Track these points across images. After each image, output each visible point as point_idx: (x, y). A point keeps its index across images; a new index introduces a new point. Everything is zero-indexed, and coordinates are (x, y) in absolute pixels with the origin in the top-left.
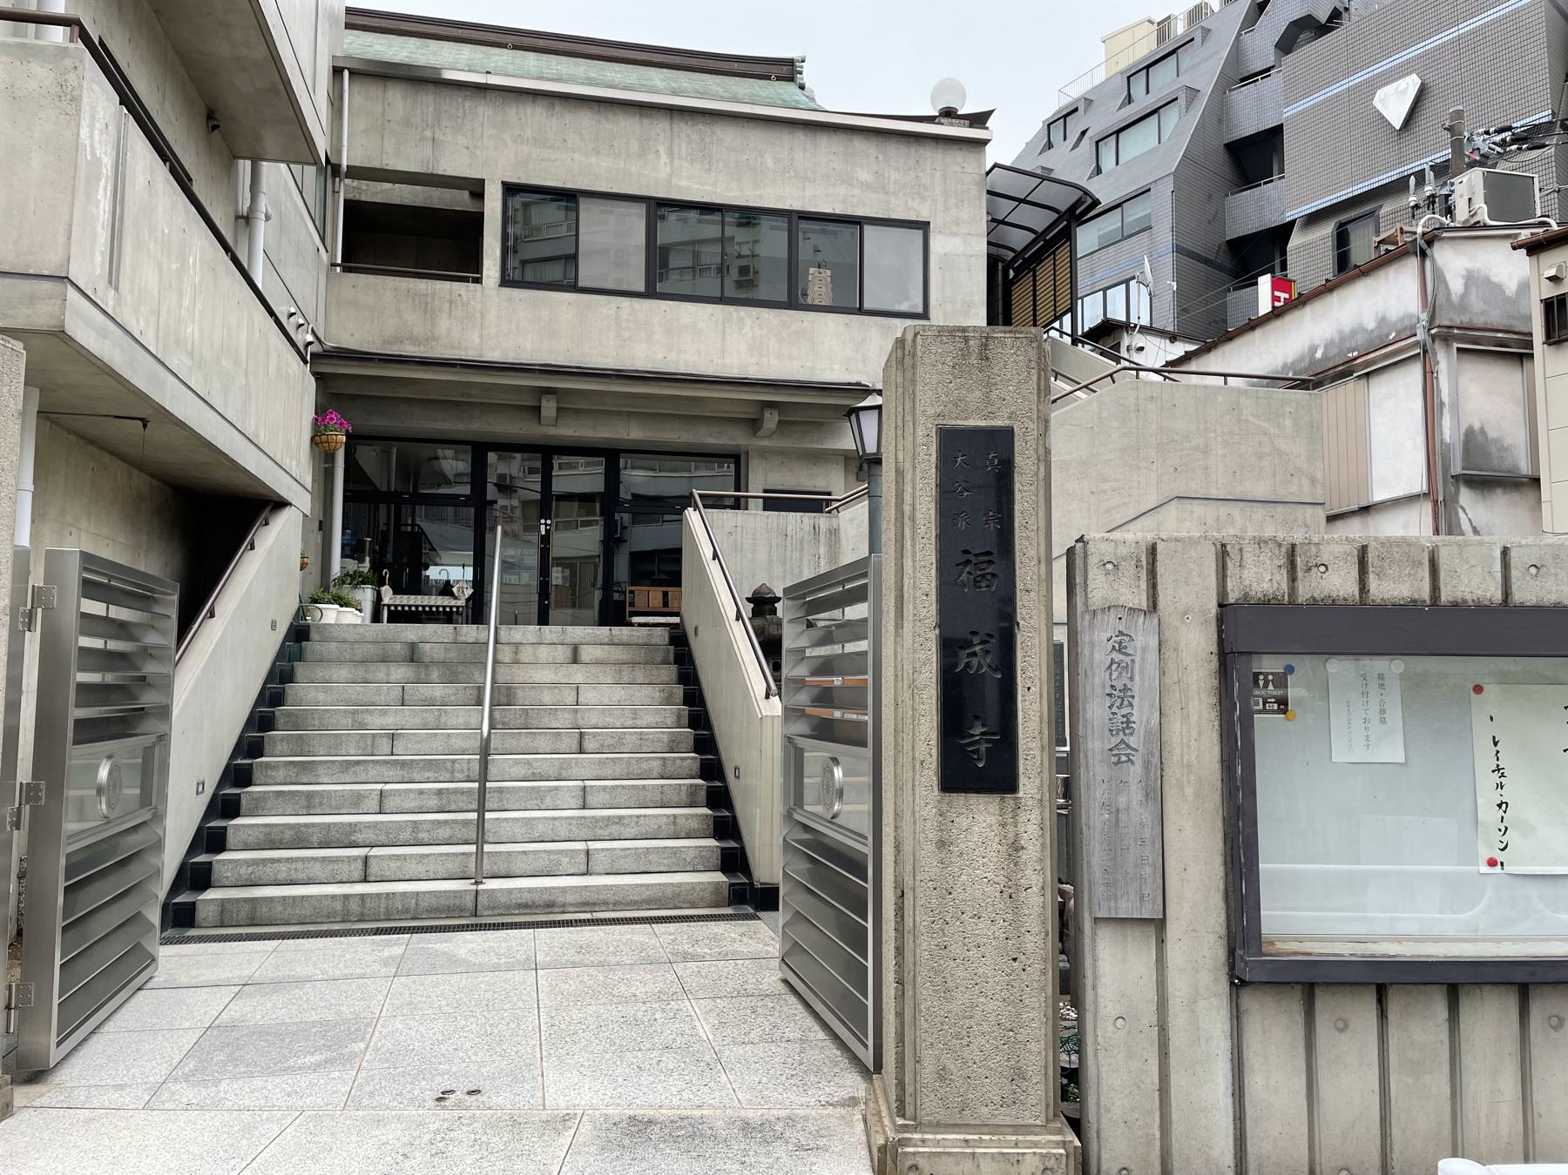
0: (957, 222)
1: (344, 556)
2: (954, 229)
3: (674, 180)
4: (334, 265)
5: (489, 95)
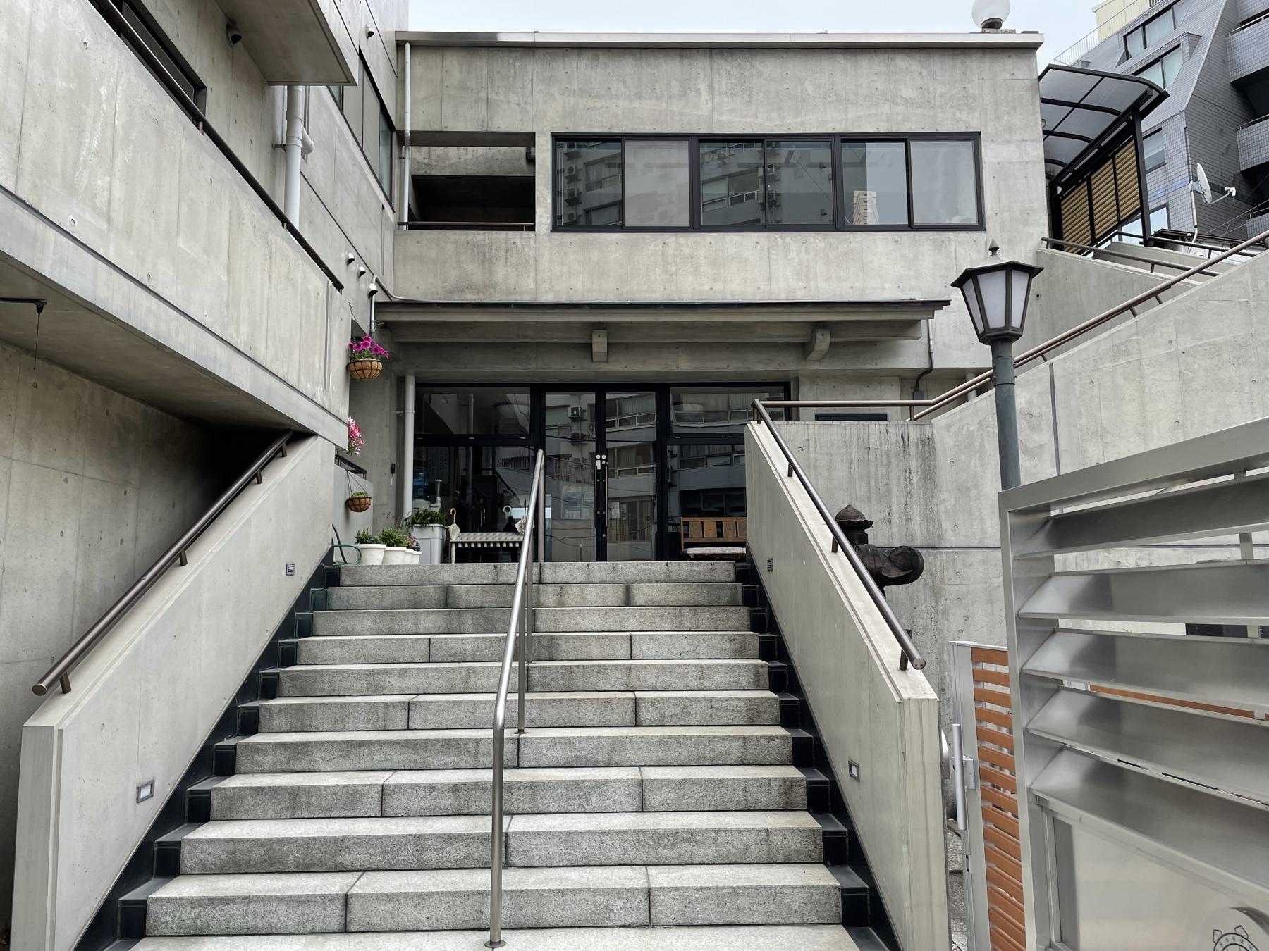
0: (1010, 130)
1: (416, 496)
2: (1007, 137)
3: (716, 116)
4: (401, 224)
5: (539, 53)
